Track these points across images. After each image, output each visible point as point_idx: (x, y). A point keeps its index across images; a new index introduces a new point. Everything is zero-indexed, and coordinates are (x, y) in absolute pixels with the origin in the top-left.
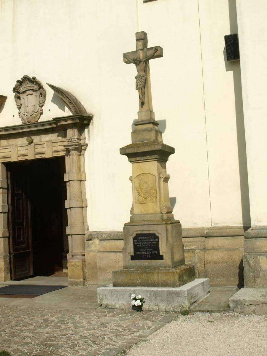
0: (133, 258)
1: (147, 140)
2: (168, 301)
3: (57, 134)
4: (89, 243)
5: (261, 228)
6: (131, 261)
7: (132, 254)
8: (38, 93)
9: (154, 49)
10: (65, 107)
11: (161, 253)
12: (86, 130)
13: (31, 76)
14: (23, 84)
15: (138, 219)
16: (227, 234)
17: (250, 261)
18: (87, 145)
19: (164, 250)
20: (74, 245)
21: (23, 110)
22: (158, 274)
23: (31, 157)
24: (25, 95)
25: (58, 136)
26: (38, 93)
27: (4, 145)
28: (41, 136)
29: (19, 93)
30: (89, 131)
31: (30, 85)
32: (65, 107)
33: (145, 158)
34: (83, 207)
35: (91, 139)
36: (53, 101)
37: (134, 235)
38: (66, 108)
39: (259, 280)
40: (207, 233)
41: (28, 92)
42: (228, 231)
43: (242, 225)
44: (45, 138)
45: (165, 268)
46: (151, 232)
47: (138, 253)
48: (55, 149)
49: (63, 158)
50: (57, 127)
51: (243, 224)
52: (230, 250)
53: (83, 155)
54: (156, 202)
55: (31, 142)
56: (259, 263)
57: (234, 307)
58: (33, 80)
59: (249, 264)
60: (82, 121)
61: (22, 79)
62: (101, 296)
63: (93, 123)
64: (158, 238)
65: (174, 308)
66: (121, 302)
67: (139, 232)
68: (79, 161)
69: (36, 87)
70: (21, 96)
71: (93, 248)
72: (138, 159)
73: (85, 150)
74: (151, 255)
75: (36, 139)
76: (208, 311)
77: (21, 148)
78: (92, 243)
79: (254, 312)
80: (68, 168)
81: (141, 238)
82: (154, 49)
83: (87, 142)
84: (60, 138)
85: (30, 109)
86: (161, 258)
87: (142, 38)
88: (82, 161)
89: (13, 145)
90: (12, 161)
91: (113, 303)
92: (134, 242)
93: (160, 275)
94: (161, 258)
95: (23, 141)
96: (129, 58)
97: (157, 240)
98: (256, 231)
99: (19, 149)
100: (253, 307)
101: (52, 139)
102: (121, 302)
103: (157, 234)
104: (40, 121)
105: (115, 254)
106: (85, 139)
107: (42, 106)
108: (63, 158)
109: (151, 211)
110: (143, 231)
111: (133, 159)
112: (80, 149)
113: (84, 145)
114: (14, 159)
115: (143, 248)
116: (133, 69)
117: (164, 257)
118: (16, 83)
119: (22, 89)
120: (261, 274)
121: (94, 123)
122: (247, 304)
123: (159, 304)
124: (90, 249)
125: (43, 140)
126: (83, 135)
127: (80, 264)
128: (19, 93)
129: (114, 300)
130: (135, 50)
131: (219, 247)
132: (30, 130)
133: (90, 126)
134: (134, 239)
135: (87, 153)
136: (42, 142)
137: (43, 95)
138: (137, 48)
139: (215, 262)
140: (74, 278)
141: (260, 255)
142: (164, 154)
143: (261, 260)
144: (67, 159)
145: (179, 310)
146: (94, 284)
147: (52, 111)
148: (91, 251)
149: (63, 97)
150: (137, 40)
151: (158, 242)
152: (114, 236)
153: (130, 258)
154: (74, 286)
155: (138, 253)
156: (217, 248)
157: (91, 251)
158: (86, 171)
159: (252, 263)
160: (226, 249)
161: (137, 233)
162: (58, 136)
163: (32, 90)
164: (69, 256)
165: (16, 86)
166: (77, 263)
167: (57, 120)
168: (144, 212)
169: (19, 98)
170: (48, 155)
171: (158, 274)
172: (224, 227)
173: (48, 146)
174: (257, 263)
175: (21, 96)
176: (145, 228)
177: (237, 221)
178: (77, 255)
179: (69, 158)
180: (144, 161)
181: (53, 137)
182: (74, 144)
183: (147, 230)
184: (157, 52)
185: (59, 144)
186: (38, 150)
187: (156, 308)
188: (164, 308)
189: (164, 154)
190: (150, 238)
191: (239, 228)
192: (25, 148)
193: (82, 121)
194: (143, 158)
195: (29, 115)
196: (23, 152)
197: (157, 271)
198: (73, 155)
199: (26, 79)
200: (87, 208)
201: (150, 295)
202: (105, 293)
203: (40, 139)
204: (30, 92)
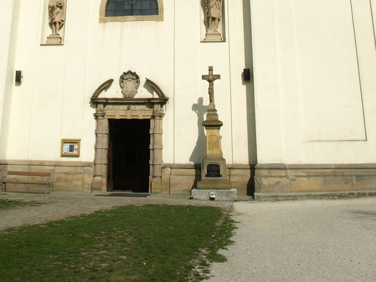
0: (206, 176)
1: (214, 119)
2: (227, 196)
3: (146, 106)
4: (164, 170)
5: (262, 165)
6: (206, 177)
7: (206, 174)
8: (135, 81)
9: (217, 76)
10: (154, 92)
11: (221, 174)
12: (164, 106)
13: (133, 71)
14: (127, 75)
15: (209, 157)
16: (241, 168)
17: (258, 180)
18: (164, 114)
19: (222, 172)
20: (154, 171)
21: (125, 89)
22: (220, 184)
23: (129, 117)
24: (126, 80)
25: (146, 107)
26: (135, 81)
27: (110, 108)
28: (136, 106)
29: (123, 79)
30: (166, 106)
31: (131, 76)
32: (154, 92)
33: (213, 128)
34: (161, 149)
35: (167, 111)
36: (144, 86)
37: (208, 165)
38: (155, 93)
39: (262, 189)
40: (231, 167)
41: (129, 80)
42: (242, 166)
43: (248, 164)
44: (138, 107)
45: (223, 181)
46: (216, 163)
47: (209, 173)
48: (144, 114)
49: (148, 121)
50: (149, 103)
51: (249, 163)
52: (243, 176)
53: (162, 119)
54: (218, 149)
55: (128, 109)
56: (262, 181)
57: (257, 199)
58: (134, 74)
59: (257, 181)
60: (163, 101)
61: (127, 72)
62: (193, 194)
63: (168, 102)
64: (219, 166)
65: (230, 199)
66: (203, 197)
67: (210, 163)
68: (160, 122)
69: (135, 78)
70: (124, 81)
71: (167, 172)
72: (210, 128)
73: (163, 117)
74: (216, 174)
75: (132, 107)
76: (245, 200)
77: (122, 112)
78: (166, 170)
79: (265, 201)
80: (152, 126)
81: (211, 166)
82: (217, 76)
83: (164, 113)
84: (148, 108)
85: (130, 89)
86: (221, 176)
87: (211, 69)
88: (161, 123)
89: (117, 109)
90: (128, 118)
91: (200, 197)
92: (207, 168)
93: (221, 184)
94: (221, 176)
95: (126, 107)
96: (204, 77)
97: (219, 167)
98: (260, 166)
99: (120, 112)
100: (265, 199)
101: (142, 108)
102: (203, 197)
103: (219, 165)
104: (136, 96)
105: (181, 176)
106: (163, 111)
107: (137, 89)
108: (148, 121)
109: (215, 153)
110: (212, 163)
111: (207, 128)
112: (161, 116)
113: (163, 114)
114: (118, 117)
115: (212, 171)
116: (207, 83)
117: (222, 176)
118: (123, 73)
119: (126, 77)
120: (263, 186)
121: (169, 102)
122: (262, 197)
123: (223, 197)
124: (164, 173)
125: (136, 108)
126: (162, 108)
127: (160, 182)
128: (123, 79)
129: (200, 196)
130: (208, 74)
131: (237, 174)
132: (128, 101)
133: (167, 104)
134: (207, 166)
135: (164, 118)
136: (136, 109)
137: (138, 82)
138: (209, 73)
139: (235, 182)
140: (155, 190)
141: (263, 177)
142: (218, 125)
143: (263, 180)
144: (152, 121)
145: (232, 200)
146: (166, 194)
147: (143, 93)
148: (165, 175)
149: (151, 85)
150: (209, 70)
151: (219, 168)
152: (180, 166)
153: (205, 175)
154: (87, 215)
155: (209, 173)
156: (236, 174)
157: (165, 175)
158: (163, 129)
159: (259, 181)
160: (241, 176)
161: (209, 163)
162: (146, 107)
163: (132, 79)
164: (150, 178)
165: (122, 75)
166: (157, 181)
167: (149, 99)
168: (212, 154)
169: (123, 82)
170: (141, 117)
171: (220, 184)
172: (239, 164)
173: (141, 112)
174: (261, 181)
175: (124, 81)
176: (214, 161)
177: (232, 163)
178: (157, 176)
179: (154, 121)
180: (213, 129)
181: (144, 107)
182: (158, 113)
183: (214, 162)
184: (218, 77)
185: (147, 112)
186: (133, 114)
187: (221, 199)
188: (225, 199)
189: (218, 125)
190: (215, 166)
191: (247, 165)
192: (125, 112)
193: (163, 101)
194: (212, 128)
195: (129, 93)
196: (123, 114)
197: (220, 182)
198: (157, 119)
199: (130, 72)
200: (163, 150)
201: (219, 193)
202: (195, 192)
203: (135, 107)
204: (130, 80)
